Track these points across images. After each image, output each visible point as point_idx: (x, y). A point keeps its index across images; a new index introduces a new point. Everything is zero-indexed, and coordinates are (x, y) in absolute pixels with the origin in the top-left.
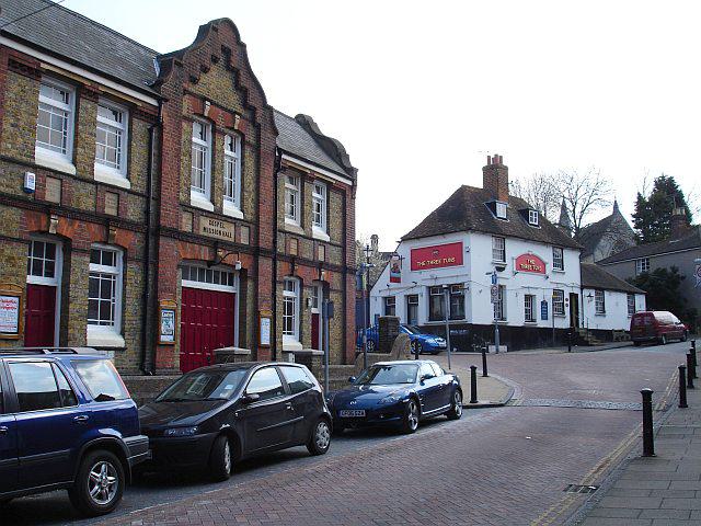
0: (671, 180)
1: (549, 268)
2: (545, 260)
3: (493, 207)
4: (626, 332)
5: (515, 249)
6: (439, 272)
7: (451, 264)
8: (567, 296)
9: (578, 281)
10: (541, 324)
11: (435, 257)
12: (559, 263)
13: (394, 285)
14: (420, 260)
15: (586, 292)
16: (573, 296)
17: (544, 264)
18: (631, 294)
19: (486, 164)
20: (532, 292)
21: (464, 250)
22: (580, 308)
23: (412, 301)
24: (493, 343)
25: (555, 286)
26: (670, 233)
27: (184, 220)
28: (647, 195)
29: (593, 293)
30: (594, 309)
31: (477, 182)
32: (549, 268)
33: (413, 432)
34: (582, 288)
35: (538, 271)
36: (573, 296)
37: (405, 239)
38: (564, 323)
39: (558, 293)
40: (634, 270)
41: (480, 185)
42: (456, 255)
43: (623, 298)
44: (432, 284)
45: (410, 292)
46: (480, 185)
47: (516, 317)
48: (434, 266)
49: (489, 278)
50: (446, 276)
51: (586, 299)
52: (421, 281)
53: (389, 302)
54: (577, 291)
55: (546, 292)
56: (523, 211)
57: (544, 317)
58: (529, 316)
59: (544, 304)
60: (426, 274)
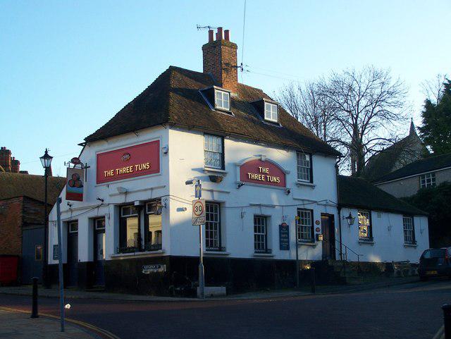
1: (292, 179)
3: (210, 96)
4: (414, 265)
5: (240, 151)
6: (128, 184)
10: (278, 254)
11: (126, 163)
12: (307, 174)
13: (76, 204)
14: (108, 168)
15: (345, 212)
19: (207, 41)
20: (266, 212)
21: (162, 151)
22: (337, 237)
23: (97, 225)
24: (64, 265)
28: (434, 101)
30: (403, 238)
31: (197, 65)
32: (292, 179)
34: (339, 207)
37: (91, 140)
38: (310, 254)
39: (304, 215)
40: (408, 187)
41: (201, 71)
42: (153, 159)
43: (396, 221)
44: (121, 200)
45: (94, 214)
46: (201, 71)
47: (239, 244)
48: (125, 176)
49: (192, 189)
50: (139, 189)
52: (110, 195)
53: (72, 225)
54: (333, 211)
56: (253, 103)
57: (284, 245)
58: (261, 242)
59: (284, 229)
60: (114, 187)
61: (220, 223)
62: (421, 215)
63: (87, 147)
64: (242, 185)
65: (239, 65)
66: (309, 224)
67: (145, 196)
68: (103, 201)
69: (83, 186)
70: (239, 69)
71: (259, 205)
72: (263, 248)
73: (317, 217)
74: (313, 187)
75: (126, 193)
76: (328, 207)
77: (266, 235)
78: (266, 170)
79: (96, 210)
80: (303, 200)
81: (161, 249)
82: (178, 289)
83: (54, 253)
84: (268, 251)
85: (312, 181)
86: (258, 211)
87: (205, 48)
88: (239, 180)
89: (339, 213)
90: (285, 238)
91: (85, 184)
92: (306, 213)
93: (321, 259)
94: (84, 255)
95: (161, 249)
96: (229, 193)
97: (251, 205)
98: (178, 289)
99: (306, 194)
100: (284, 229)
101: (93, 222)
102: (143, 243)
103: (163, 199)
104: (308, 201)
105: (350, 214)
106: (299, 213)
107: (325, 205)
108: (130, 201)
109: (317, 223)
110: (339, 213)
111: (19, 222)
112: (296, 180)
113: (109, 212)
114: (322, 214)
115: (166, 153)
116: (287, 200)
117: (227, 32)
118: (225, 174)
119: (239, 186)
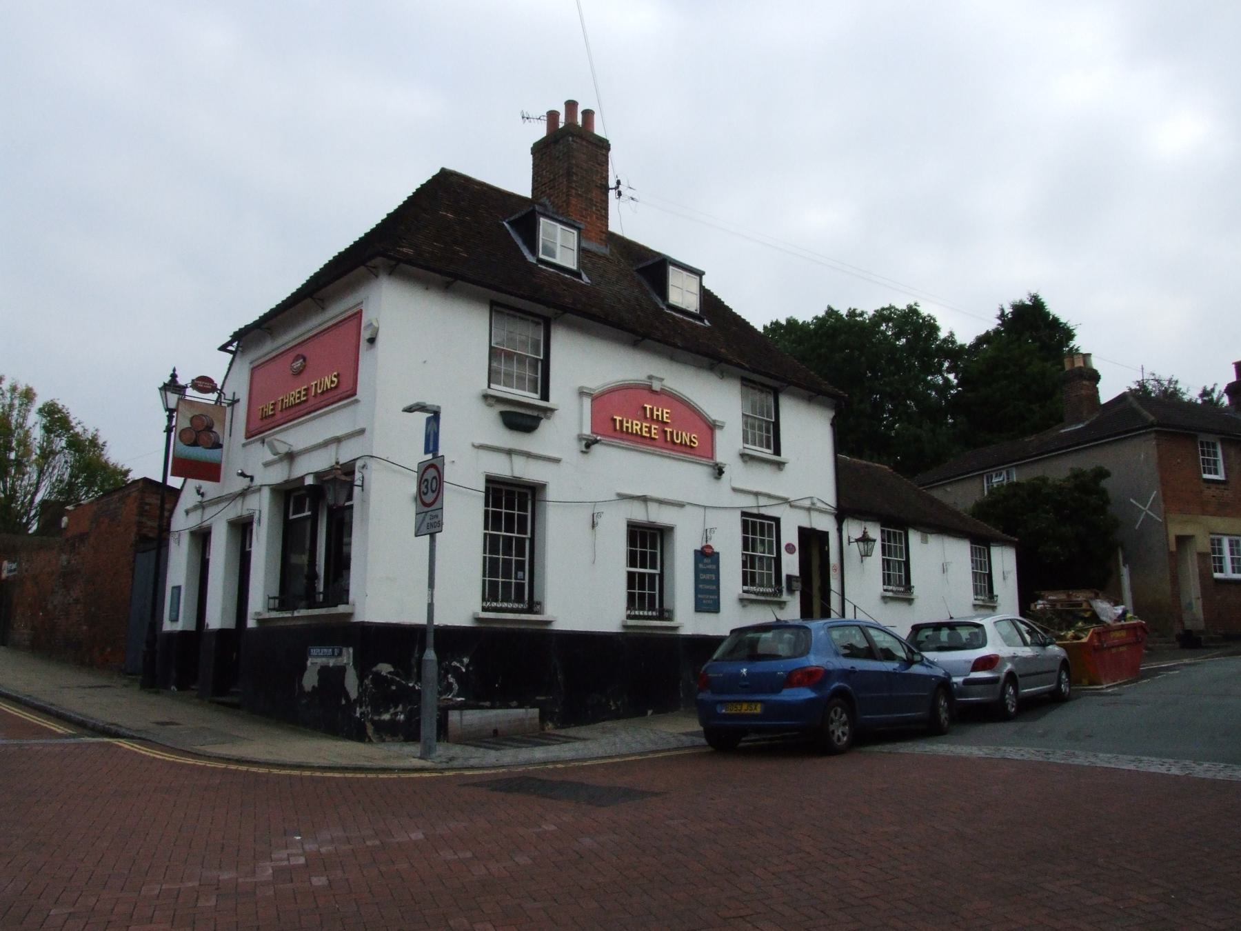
0: (1074, 336)
1: (729, 443)
2: (713, 414)
7: (487, 708)
8: (790, 536)
9: (827, 493)
15: (853, 529)
16: (812, 541)
17: (712, 427)
18: (981, 544)
25: (748, 503)
26: (457, 836)
27: (17, 618)
29: (875, 532)
32: (729, 443)
33: (511, 708)
34: (842, 514)
35: (687, 448)
36: (812, 541)
41: (530, 196)
43: (959, 553)
44: (278, 475)
46: (530, 196)
51: (853, 550)
54: (825, 523)
55: (713, 519)
57: (707, 600)
59: (706, 558)
61: (532, 540)
62: (1003, 543)
63: (239, 354)
64: (596, 442)
65: (612, 183)
66: (770, 552)
67: (320, 462)
68: (252, 478)
69: (220, 446)
70: (612, 194)
71: (644, 499)
72: (520, 598)
73: (790, 536)
74: (780, 465)
75: (291, 457)
76: (814, 514)
77: (661, 575)
78: (664, 414)
79: (239, 501)
80: (757, 494)
81: (347, 603)
82: (386, 717)
83: (171, 610)
84: (665, 613)
85: (777, 451)
86: (639, 514)
87: (539, 150)
88: (587, 431)
89: (840, 530)
90: (705, 582)
91: (225, 441)
92: (762, 525)
93: (285, 461)
94: (216, 618)
95: (347, 603)
96: (557, 461)
97: (623, 497)
98: (386, 717)
99: (762, 479)
100: (706, 558)
101: (666, 606)
102: (321, 587)
103: (359, 464)
104: (769, 496)
105: (865, 533)
106: (745, 525)
107: (809, 509)
108: (299, 476)
109: (790, 549)
110: (840, 530)
111: (133, 537)
112: (739, 445)
113: (261, 506)
114: (802, 531)
115: (372, 341)
116: (721, 493)
117: (588, 114)
118: (549, 411)
119: (588, 446)
